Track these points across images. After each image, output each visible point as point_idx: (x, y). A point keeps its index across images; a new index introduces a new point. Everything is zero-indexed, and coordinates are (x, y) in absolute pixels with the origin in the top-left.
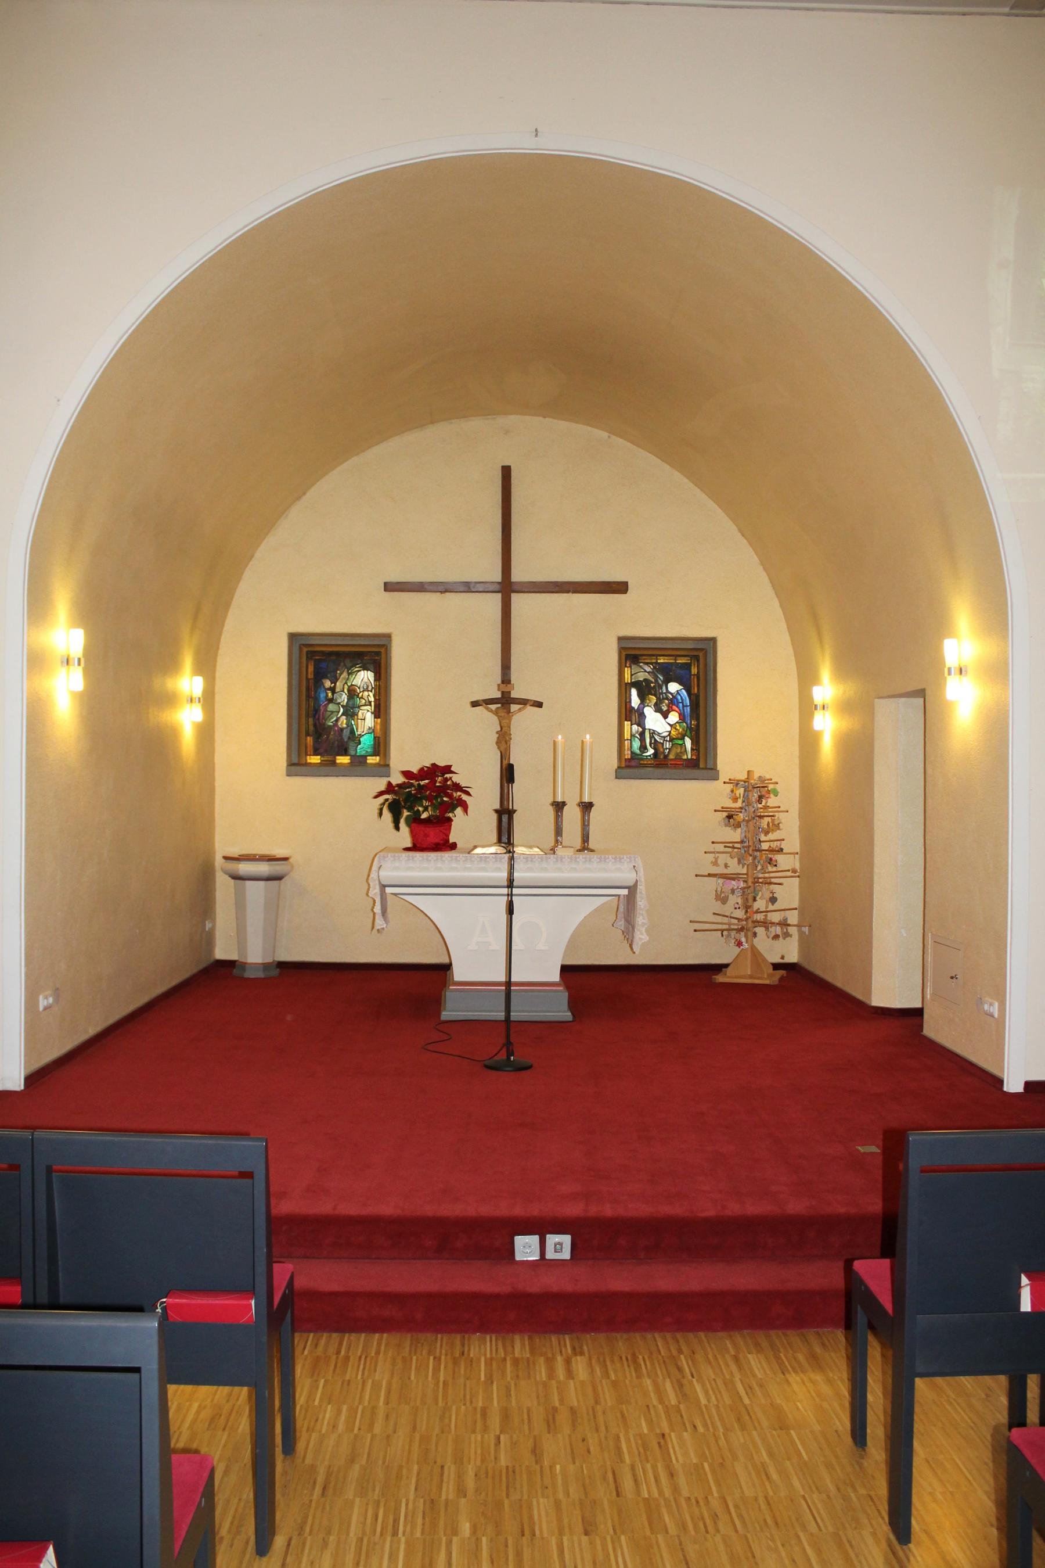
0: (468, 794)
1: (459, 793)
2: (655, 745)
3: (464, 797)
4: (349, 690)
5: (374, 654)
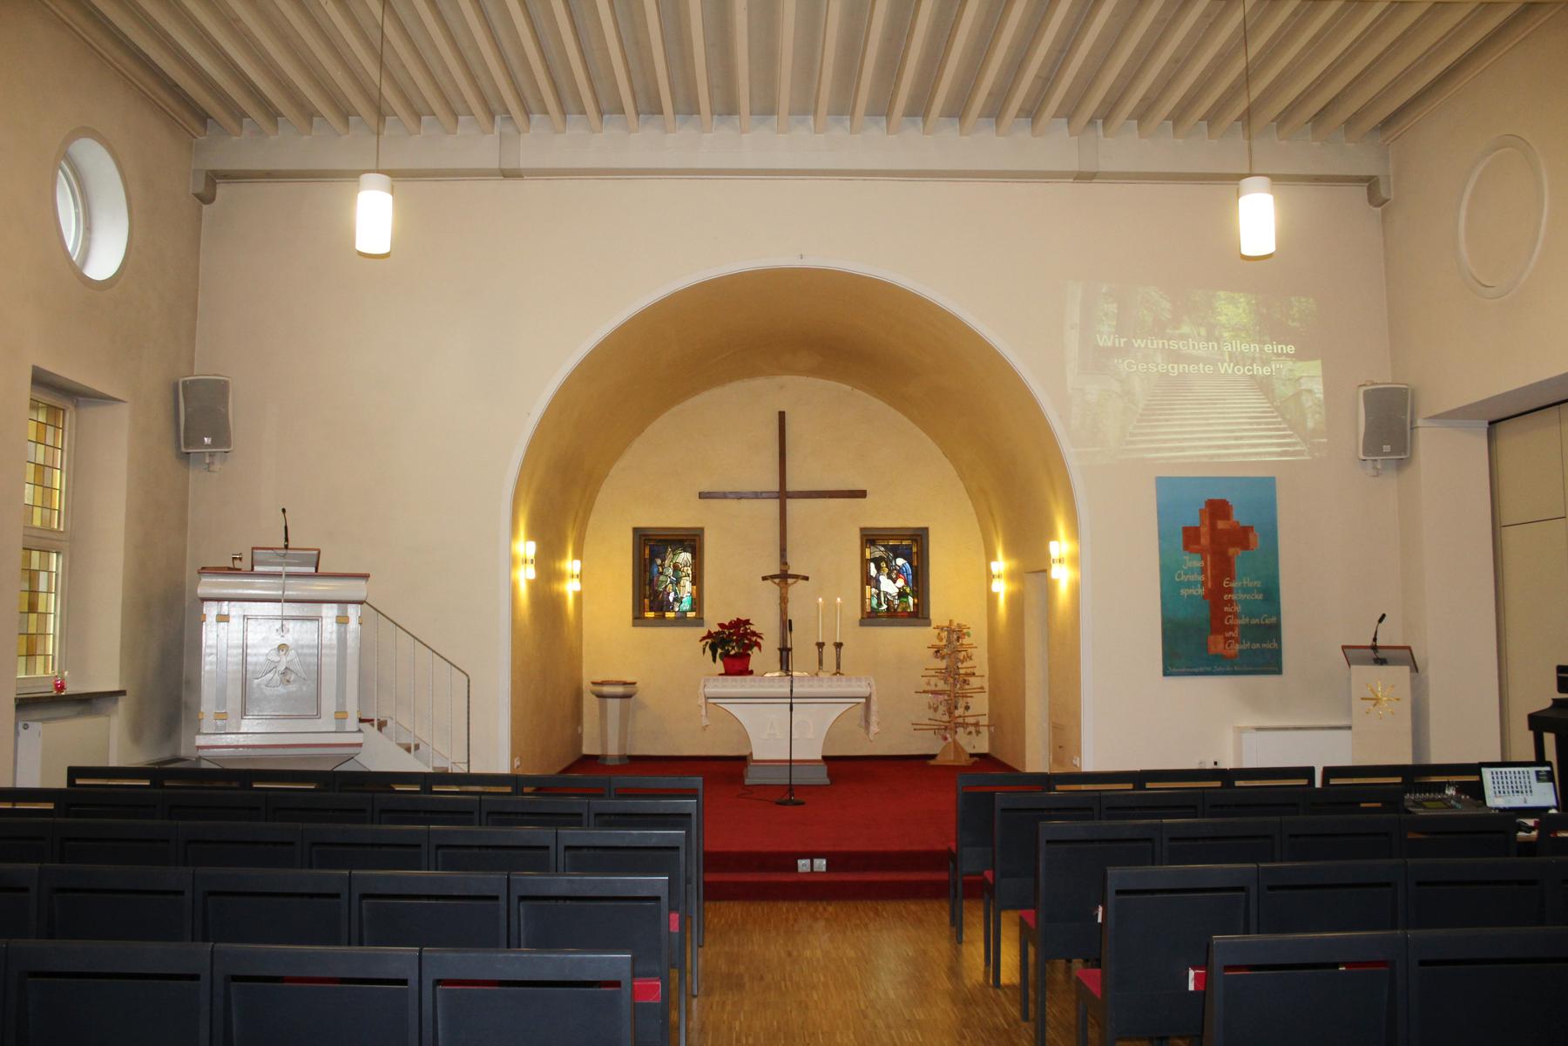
5: (691, 541)
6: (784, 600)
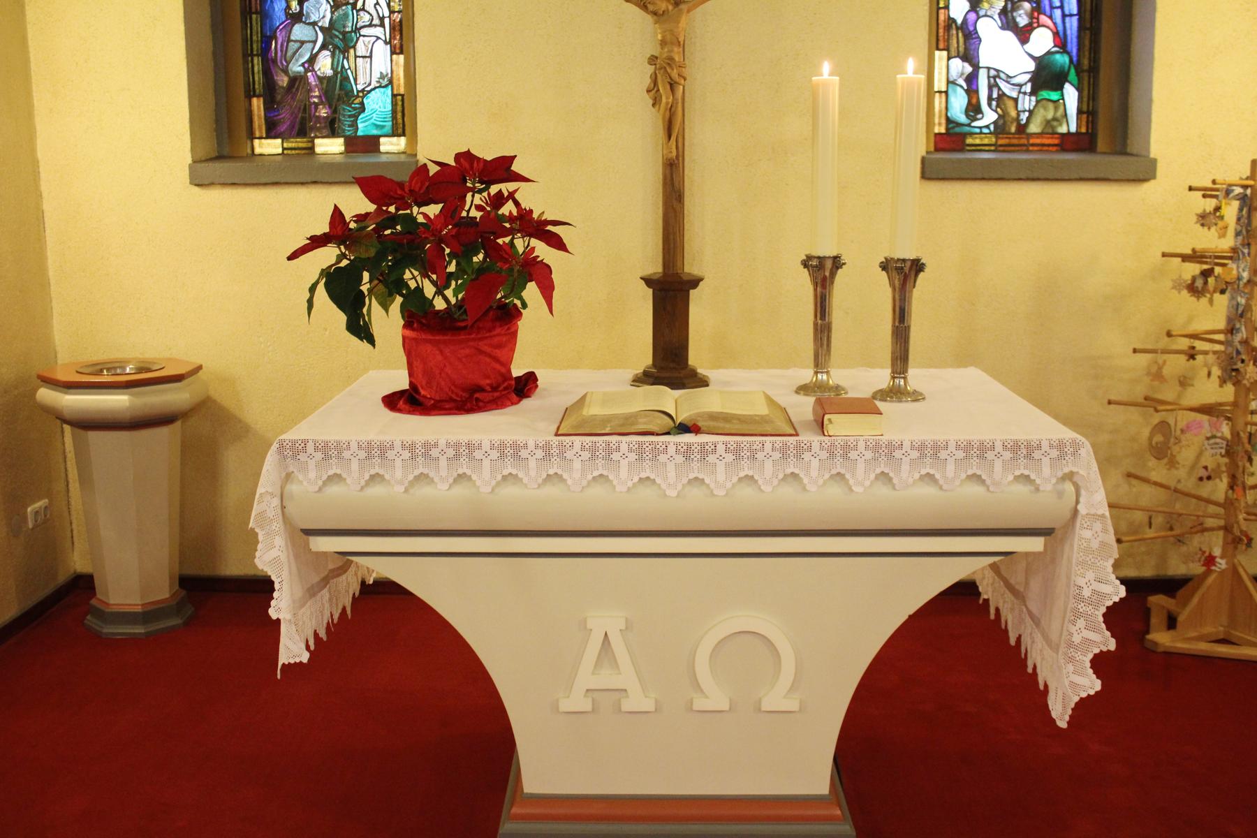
0: (557, 243)
1: (534, 242)
2: (1000, 100)
3: (542, 251)
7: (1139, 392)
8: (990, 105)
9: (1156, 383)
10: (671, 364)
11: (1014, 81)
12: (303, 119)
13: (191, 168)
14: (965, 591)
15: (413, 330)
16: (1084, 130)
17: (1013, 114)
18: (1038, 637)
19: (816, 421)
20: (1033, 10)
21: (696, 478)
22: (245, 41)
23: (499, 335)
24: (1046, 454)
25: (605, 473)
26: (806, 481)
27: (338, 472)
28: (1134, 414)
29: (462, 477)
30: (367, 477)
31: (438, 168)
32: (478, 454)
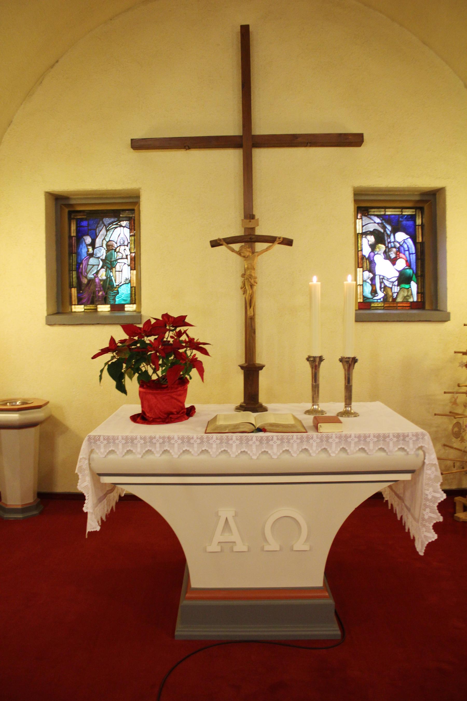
0: (205, 352)
1: (195, 352)
3: (199, 356)
4: (107, 246)
5: (124, 209)
6: (248, 282)
7: (447, 409)
8: (381, 290)
9: (454, 406)
10: (251, 402)
11: (391, 280)
12: (93, 297)
13: (46, 317)
14: (378, 496)
15: (144, 388)
16: (420, 300)
17: (390, 294)
18: (410, 516)
19: (314, 426)
20: (397, 251)
21: (265, 451)
22: (70, 264)
23: (180, 390)
24: (411, 439)
25: (226, 449)
26: (311, 452)
27: (113, 449)
28: (445, 419)
29: (165, 451)
30: (125, 451)
31: (155, 321)
32: (172, 441)
